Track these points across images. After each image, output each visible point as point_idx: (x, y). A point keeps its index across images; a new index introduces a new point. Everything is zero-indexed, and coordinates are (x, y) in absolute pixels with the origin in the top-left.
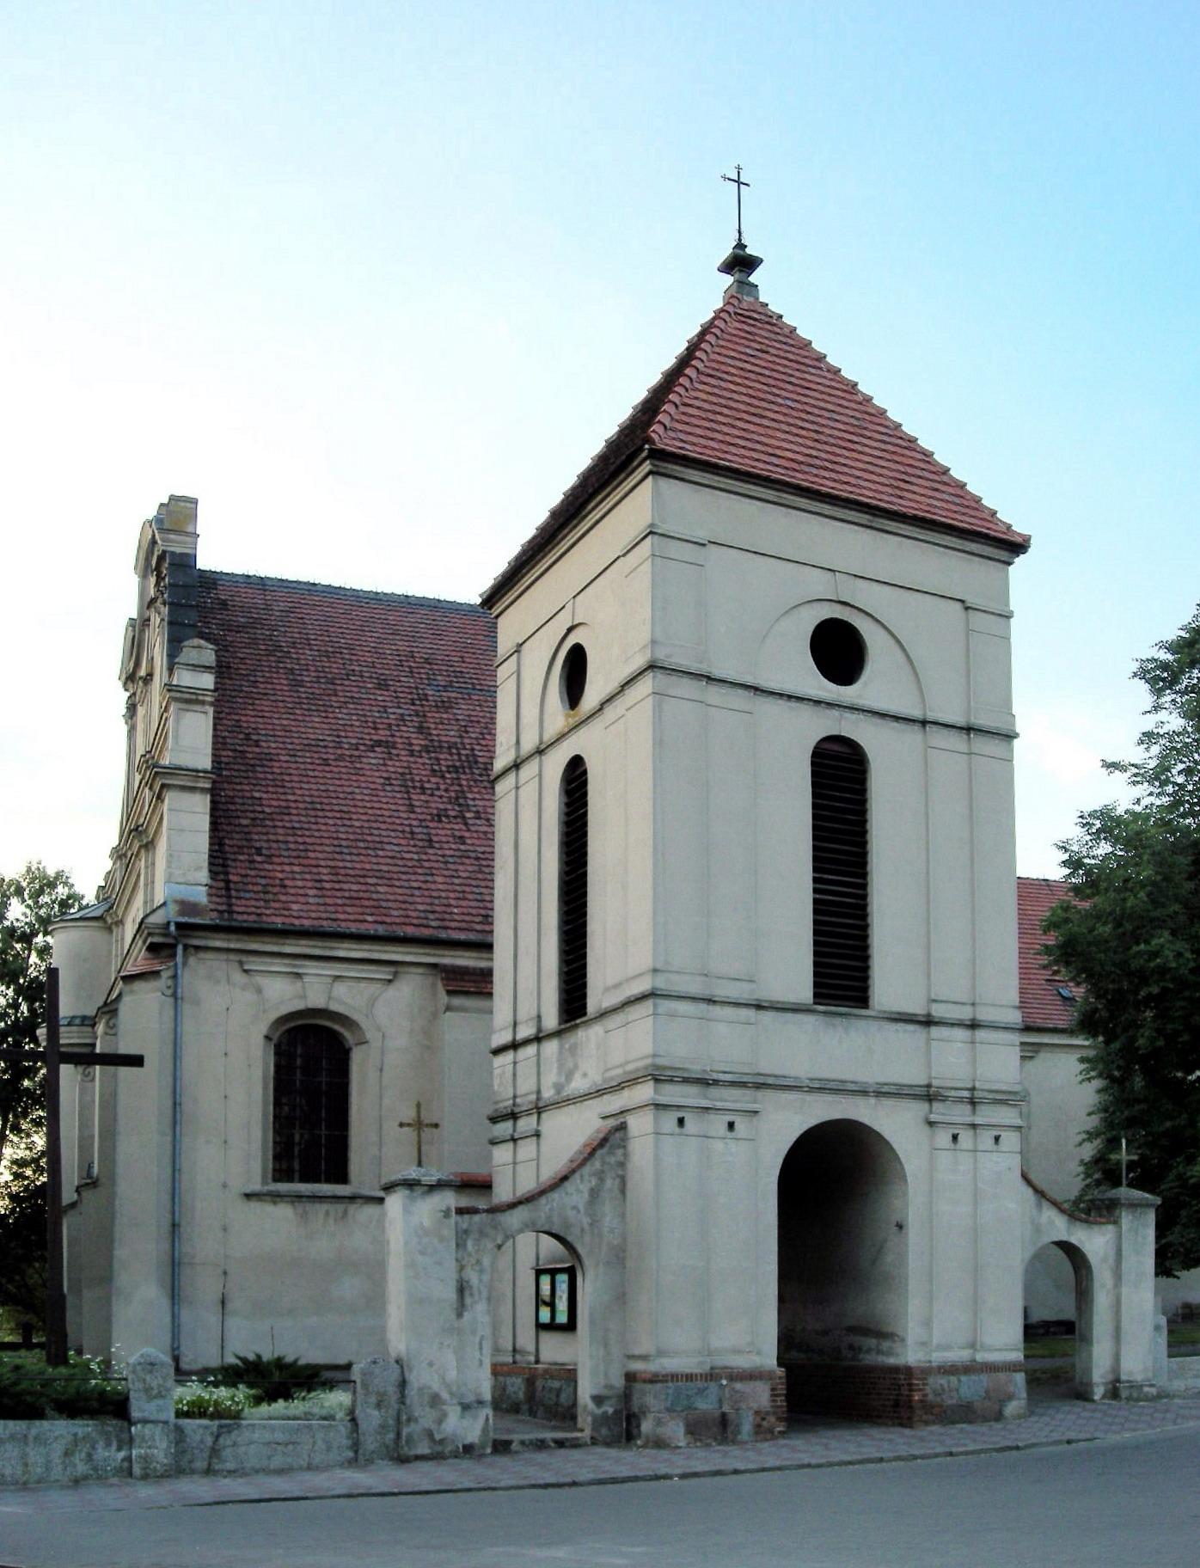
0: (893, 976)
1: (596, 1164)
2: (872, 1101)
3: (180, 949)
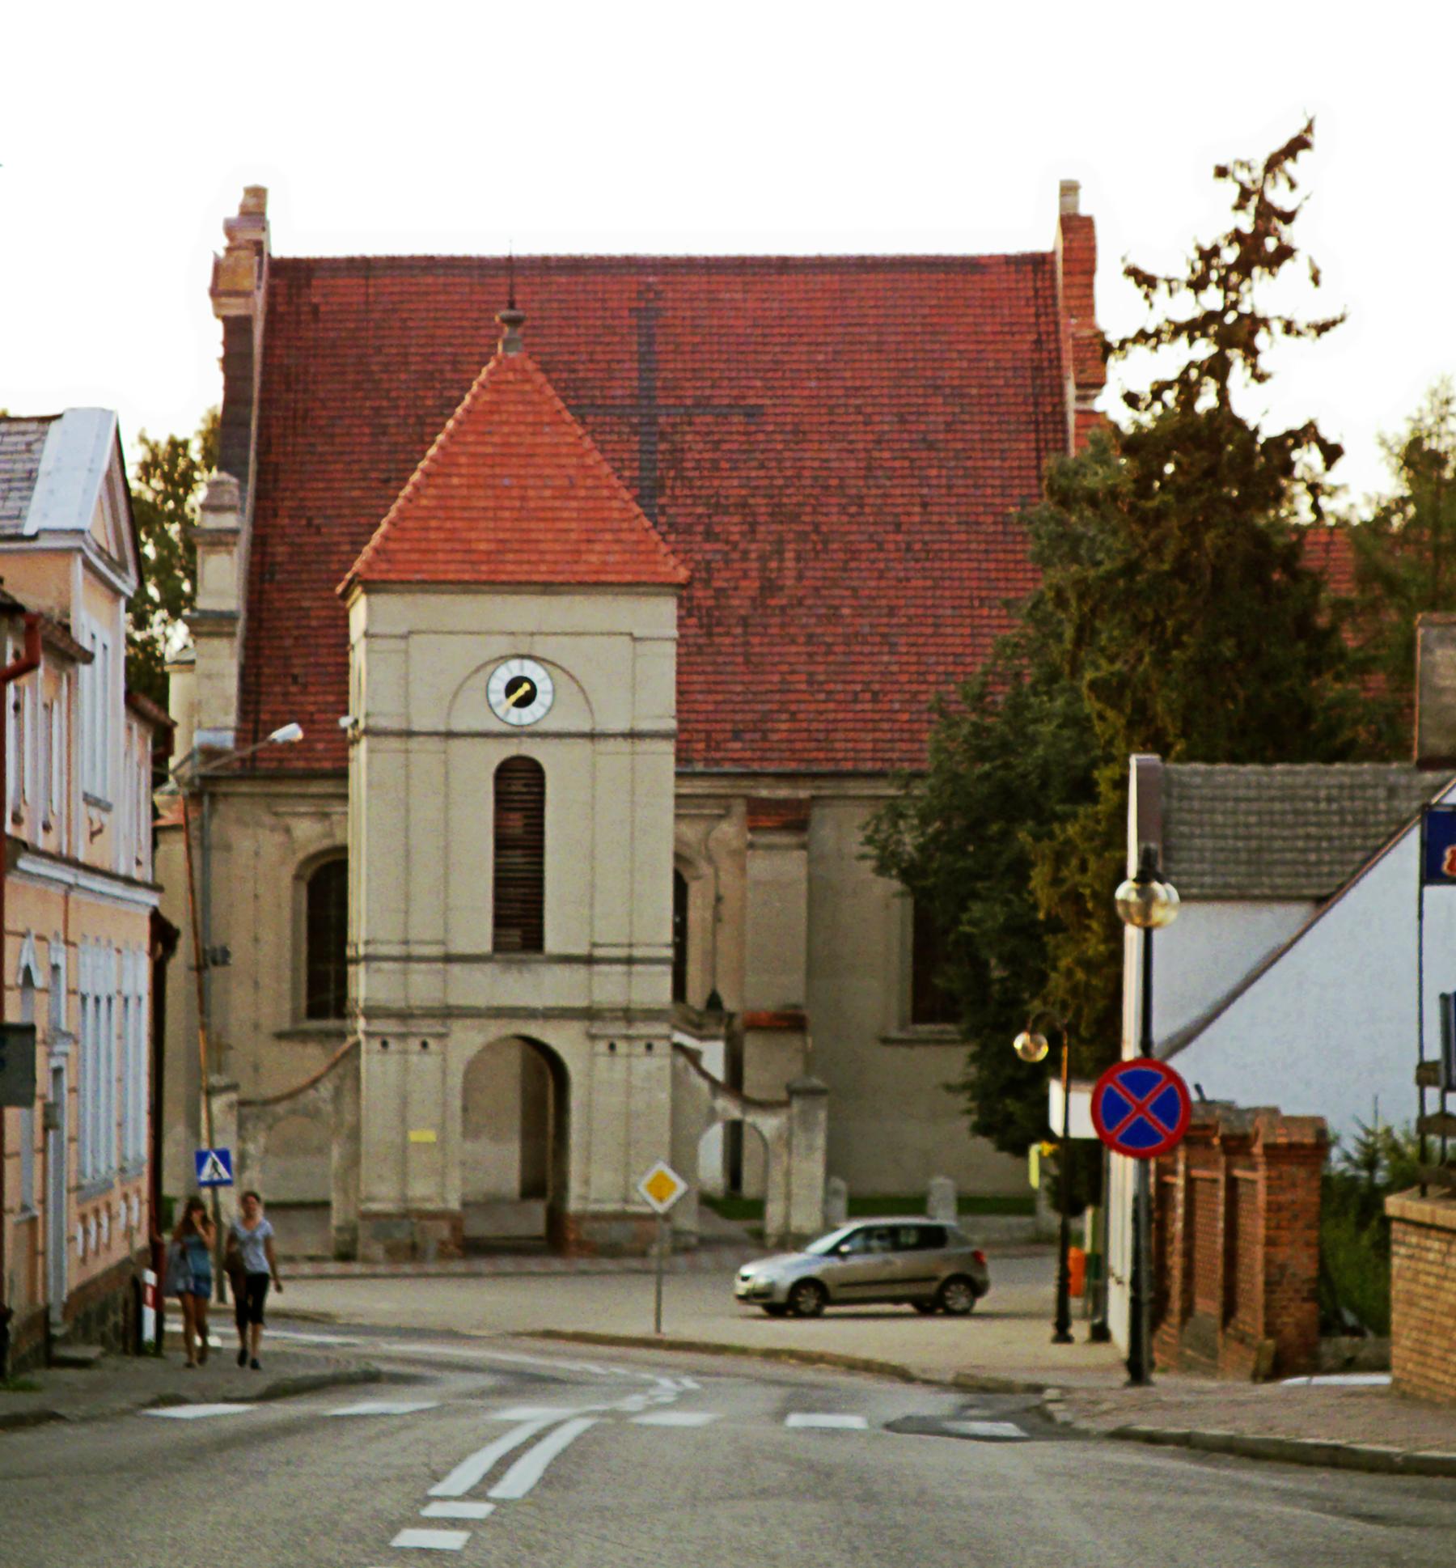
1: (340, 1070)
3: (206, 800)
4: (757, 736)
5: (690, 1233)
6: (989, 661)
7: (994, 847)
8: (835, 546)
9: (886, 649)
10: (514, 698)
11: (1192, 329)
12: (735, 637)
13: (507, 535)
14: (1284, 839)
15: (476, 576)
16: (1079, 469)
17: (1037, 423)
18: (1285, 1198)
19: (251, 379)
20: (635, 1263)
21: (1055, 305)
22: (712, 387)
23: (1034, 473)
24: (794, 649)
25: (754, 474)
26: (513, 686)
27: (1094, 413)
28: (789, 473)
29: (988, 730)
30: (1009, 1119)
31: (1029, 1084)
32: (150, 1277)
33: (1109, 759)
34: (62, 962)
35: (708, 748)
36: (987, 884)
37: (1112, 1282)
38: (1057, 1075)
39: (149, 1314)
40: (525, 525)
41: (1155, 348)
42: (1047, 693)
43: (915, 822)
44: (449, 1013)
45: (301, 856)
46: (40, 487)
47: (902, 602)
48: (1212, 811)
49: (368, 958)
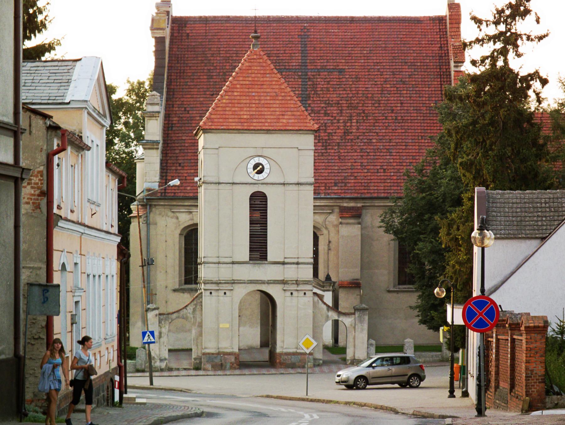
0: (274, 251)
2: (266, 285)
3: (148, 207)
4: (343, 185)
5: (321, 359)
6: (424, 158)
7: (427, 223)
8: (370, 118)
9: (388, 154)
10: (256, 171)
11: (494, 38)
12: (335, 150)
13: (254, 113)
14: (530, 217)
15: (243, 128)
16: (456, 89)
17: (441, 75)
18: (531, 346)
19: (165, 58)
20: (300, 370)
21: (446, 34)
22: (327, 62)
23: (440, 92)
24: (356, 154)
25: (341, 92)
26: (255, 167)
27: (461, 71)
28: (354, 92)
29: (424, 182)
30: (432, 318)
31: (439, 306)
32: (117, 378)
33: (467, 191)
34: (79, 262)
35: (325, 189)
36: (424, 236)
37: (469, 376)
38: (450, 303)
39: (117, 392)
40: (260, 109)
41: (482, 45)
42: (445, 169)
43: (399, 214)
44: (233, 282)
45: (182, 227)
46: (72, 85)
47: (394, 137)
48: (504, 207)
49: (204, 263)
